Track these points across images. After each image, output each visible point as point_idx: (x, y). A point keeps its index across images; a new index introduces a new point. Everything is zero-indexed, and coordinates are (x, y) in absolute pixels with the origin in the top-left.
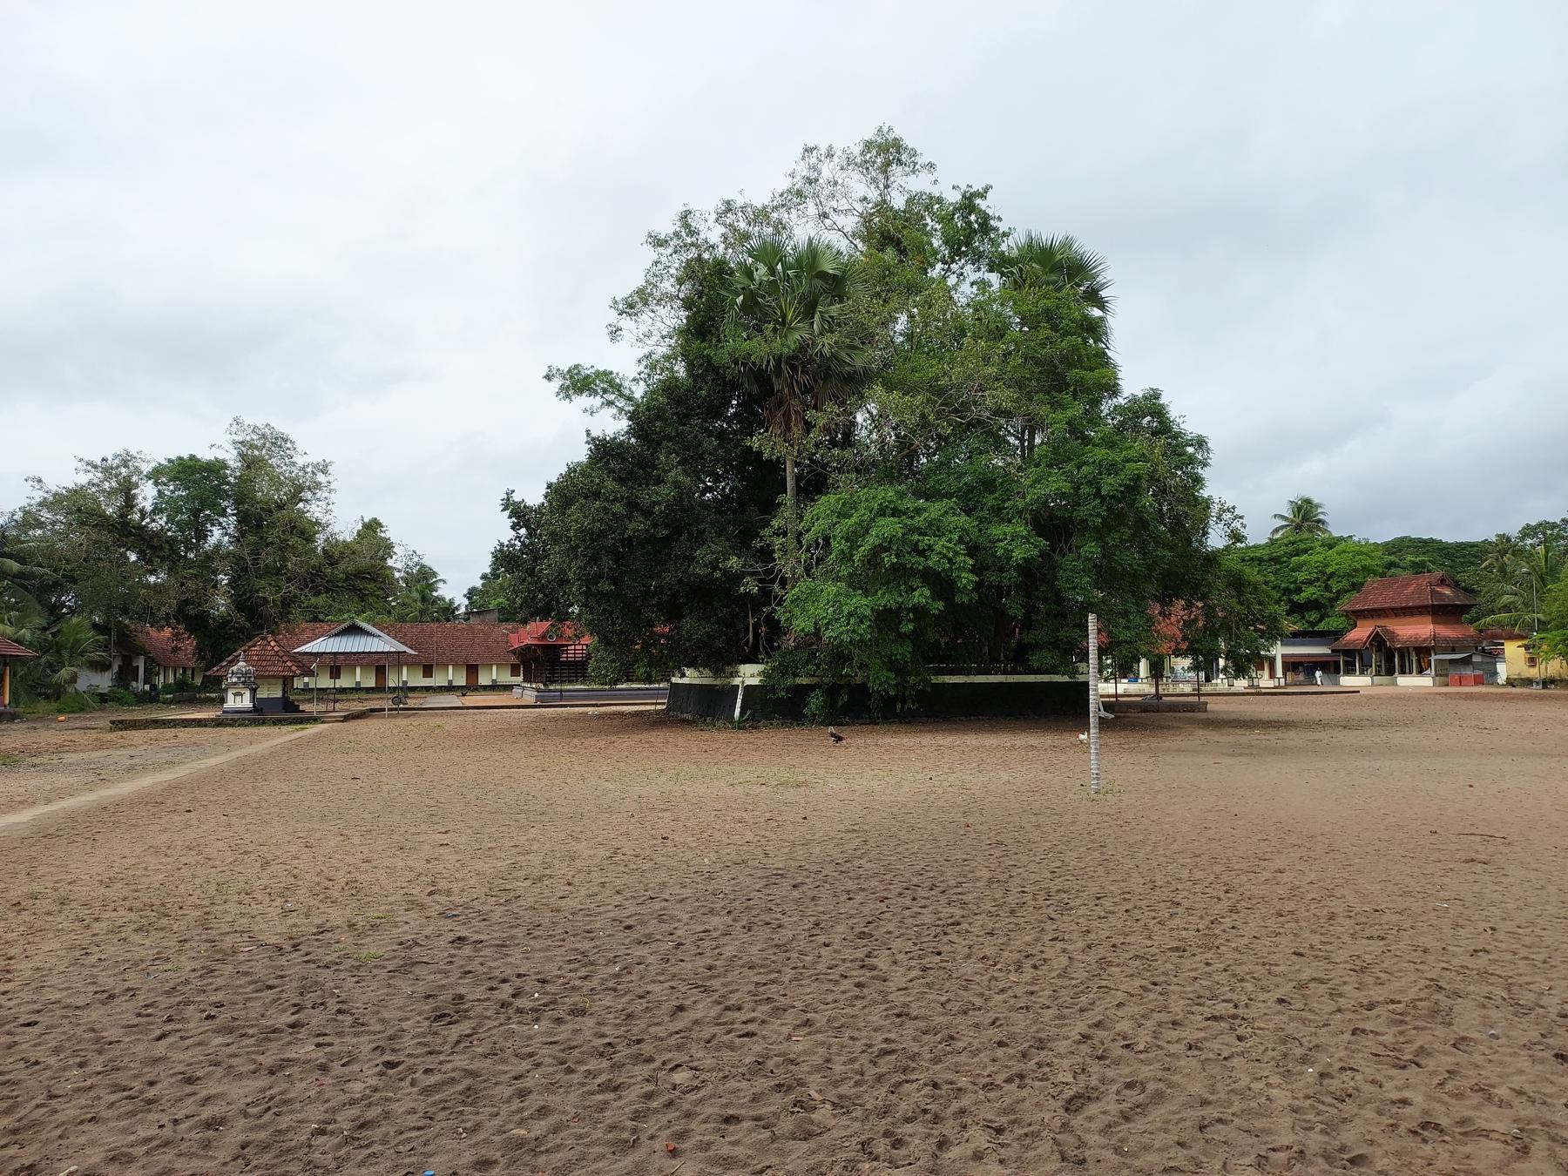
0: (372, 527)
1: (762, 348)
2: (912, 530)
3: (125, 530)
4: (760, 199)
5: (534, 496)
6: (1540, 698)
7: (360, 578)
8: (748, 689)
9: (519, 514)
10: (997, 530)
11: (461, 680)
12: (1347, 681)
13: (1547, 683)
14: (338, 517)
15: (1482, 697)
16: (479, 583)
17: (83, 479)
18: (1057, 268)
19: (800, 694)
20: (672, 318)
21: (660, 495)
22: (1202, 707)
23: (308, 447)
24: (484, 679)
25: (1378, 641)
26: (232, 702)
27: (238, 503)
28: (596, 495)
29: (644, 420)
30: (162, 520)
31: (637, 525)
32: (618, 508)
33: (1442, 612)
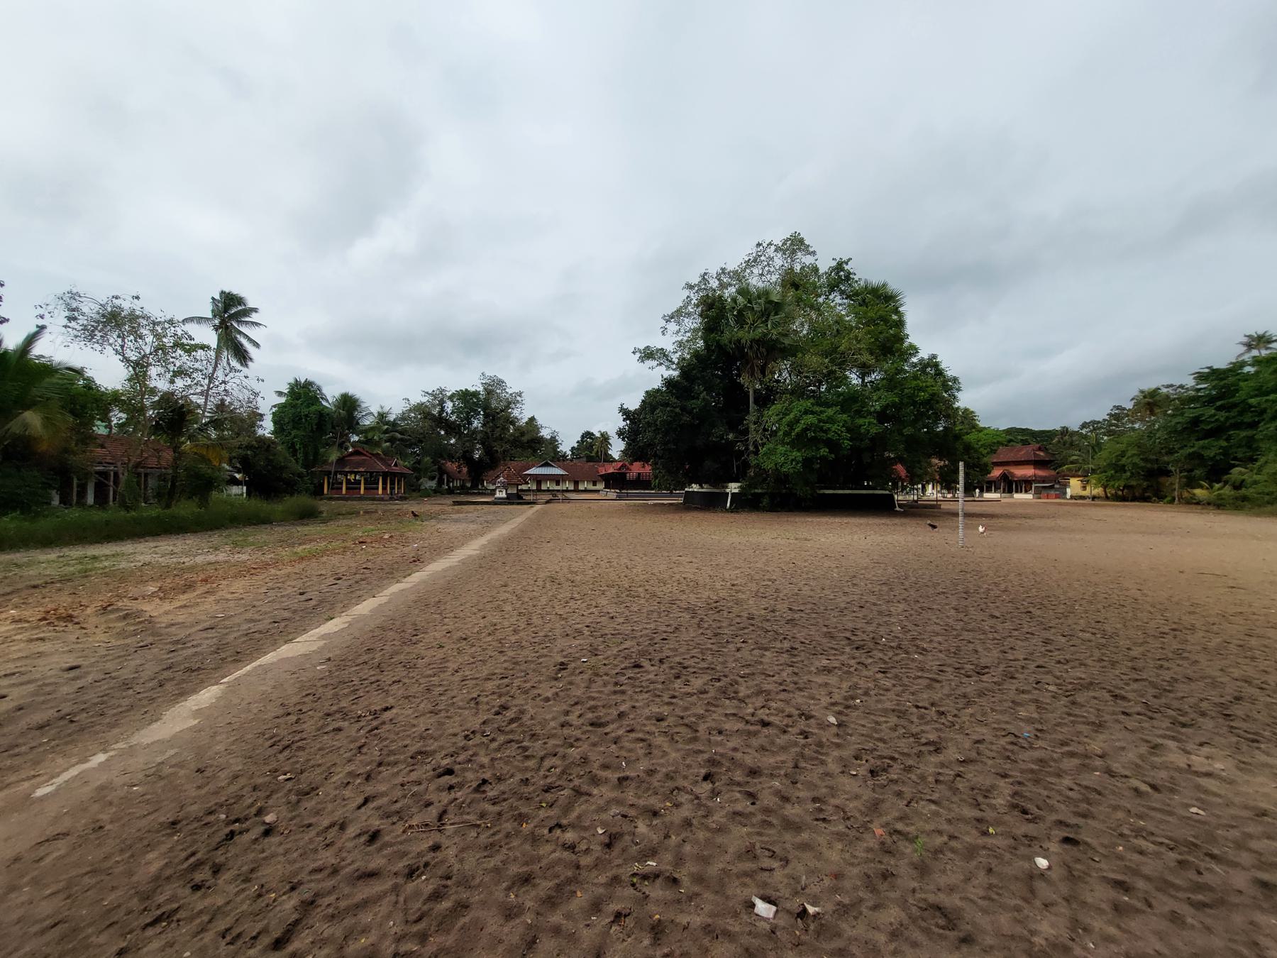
0: (532, 419)
1: (746, 335)
2: (820, 421)
3: (440, 421)
4: (731, 267)
5: (634, 404)
6: (1090, 505)
7: (532, 443)
8: (733, 494)
9: (626, 413)
10: (861, 421)
11: (572, 488)
12: (987, 496)
13: (1094, 498)
14: (522, 414)
15: (1060, 504)
16: (1129, 405)
17: (424, 399)
18: (879, 297)
19: (758, 497)
20: (693, 323)
21: (695, 404)
22: (938, 507)
23: (512, 387)
24: (581, 487)
25: (1004, 477)
26: (498, 495)
27: (484, 410)
28: (667, 405)
29: (687, 370)
30: (454, 417)
31: (686, 418)
32: (678, 410)
33: (1038, 464)
